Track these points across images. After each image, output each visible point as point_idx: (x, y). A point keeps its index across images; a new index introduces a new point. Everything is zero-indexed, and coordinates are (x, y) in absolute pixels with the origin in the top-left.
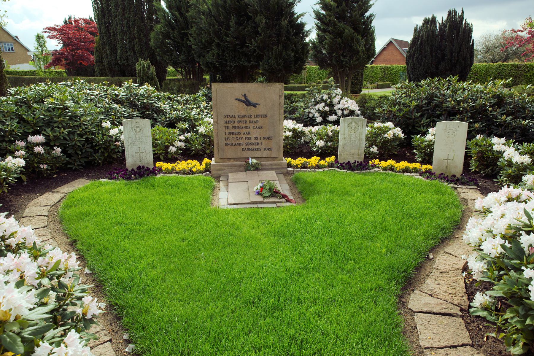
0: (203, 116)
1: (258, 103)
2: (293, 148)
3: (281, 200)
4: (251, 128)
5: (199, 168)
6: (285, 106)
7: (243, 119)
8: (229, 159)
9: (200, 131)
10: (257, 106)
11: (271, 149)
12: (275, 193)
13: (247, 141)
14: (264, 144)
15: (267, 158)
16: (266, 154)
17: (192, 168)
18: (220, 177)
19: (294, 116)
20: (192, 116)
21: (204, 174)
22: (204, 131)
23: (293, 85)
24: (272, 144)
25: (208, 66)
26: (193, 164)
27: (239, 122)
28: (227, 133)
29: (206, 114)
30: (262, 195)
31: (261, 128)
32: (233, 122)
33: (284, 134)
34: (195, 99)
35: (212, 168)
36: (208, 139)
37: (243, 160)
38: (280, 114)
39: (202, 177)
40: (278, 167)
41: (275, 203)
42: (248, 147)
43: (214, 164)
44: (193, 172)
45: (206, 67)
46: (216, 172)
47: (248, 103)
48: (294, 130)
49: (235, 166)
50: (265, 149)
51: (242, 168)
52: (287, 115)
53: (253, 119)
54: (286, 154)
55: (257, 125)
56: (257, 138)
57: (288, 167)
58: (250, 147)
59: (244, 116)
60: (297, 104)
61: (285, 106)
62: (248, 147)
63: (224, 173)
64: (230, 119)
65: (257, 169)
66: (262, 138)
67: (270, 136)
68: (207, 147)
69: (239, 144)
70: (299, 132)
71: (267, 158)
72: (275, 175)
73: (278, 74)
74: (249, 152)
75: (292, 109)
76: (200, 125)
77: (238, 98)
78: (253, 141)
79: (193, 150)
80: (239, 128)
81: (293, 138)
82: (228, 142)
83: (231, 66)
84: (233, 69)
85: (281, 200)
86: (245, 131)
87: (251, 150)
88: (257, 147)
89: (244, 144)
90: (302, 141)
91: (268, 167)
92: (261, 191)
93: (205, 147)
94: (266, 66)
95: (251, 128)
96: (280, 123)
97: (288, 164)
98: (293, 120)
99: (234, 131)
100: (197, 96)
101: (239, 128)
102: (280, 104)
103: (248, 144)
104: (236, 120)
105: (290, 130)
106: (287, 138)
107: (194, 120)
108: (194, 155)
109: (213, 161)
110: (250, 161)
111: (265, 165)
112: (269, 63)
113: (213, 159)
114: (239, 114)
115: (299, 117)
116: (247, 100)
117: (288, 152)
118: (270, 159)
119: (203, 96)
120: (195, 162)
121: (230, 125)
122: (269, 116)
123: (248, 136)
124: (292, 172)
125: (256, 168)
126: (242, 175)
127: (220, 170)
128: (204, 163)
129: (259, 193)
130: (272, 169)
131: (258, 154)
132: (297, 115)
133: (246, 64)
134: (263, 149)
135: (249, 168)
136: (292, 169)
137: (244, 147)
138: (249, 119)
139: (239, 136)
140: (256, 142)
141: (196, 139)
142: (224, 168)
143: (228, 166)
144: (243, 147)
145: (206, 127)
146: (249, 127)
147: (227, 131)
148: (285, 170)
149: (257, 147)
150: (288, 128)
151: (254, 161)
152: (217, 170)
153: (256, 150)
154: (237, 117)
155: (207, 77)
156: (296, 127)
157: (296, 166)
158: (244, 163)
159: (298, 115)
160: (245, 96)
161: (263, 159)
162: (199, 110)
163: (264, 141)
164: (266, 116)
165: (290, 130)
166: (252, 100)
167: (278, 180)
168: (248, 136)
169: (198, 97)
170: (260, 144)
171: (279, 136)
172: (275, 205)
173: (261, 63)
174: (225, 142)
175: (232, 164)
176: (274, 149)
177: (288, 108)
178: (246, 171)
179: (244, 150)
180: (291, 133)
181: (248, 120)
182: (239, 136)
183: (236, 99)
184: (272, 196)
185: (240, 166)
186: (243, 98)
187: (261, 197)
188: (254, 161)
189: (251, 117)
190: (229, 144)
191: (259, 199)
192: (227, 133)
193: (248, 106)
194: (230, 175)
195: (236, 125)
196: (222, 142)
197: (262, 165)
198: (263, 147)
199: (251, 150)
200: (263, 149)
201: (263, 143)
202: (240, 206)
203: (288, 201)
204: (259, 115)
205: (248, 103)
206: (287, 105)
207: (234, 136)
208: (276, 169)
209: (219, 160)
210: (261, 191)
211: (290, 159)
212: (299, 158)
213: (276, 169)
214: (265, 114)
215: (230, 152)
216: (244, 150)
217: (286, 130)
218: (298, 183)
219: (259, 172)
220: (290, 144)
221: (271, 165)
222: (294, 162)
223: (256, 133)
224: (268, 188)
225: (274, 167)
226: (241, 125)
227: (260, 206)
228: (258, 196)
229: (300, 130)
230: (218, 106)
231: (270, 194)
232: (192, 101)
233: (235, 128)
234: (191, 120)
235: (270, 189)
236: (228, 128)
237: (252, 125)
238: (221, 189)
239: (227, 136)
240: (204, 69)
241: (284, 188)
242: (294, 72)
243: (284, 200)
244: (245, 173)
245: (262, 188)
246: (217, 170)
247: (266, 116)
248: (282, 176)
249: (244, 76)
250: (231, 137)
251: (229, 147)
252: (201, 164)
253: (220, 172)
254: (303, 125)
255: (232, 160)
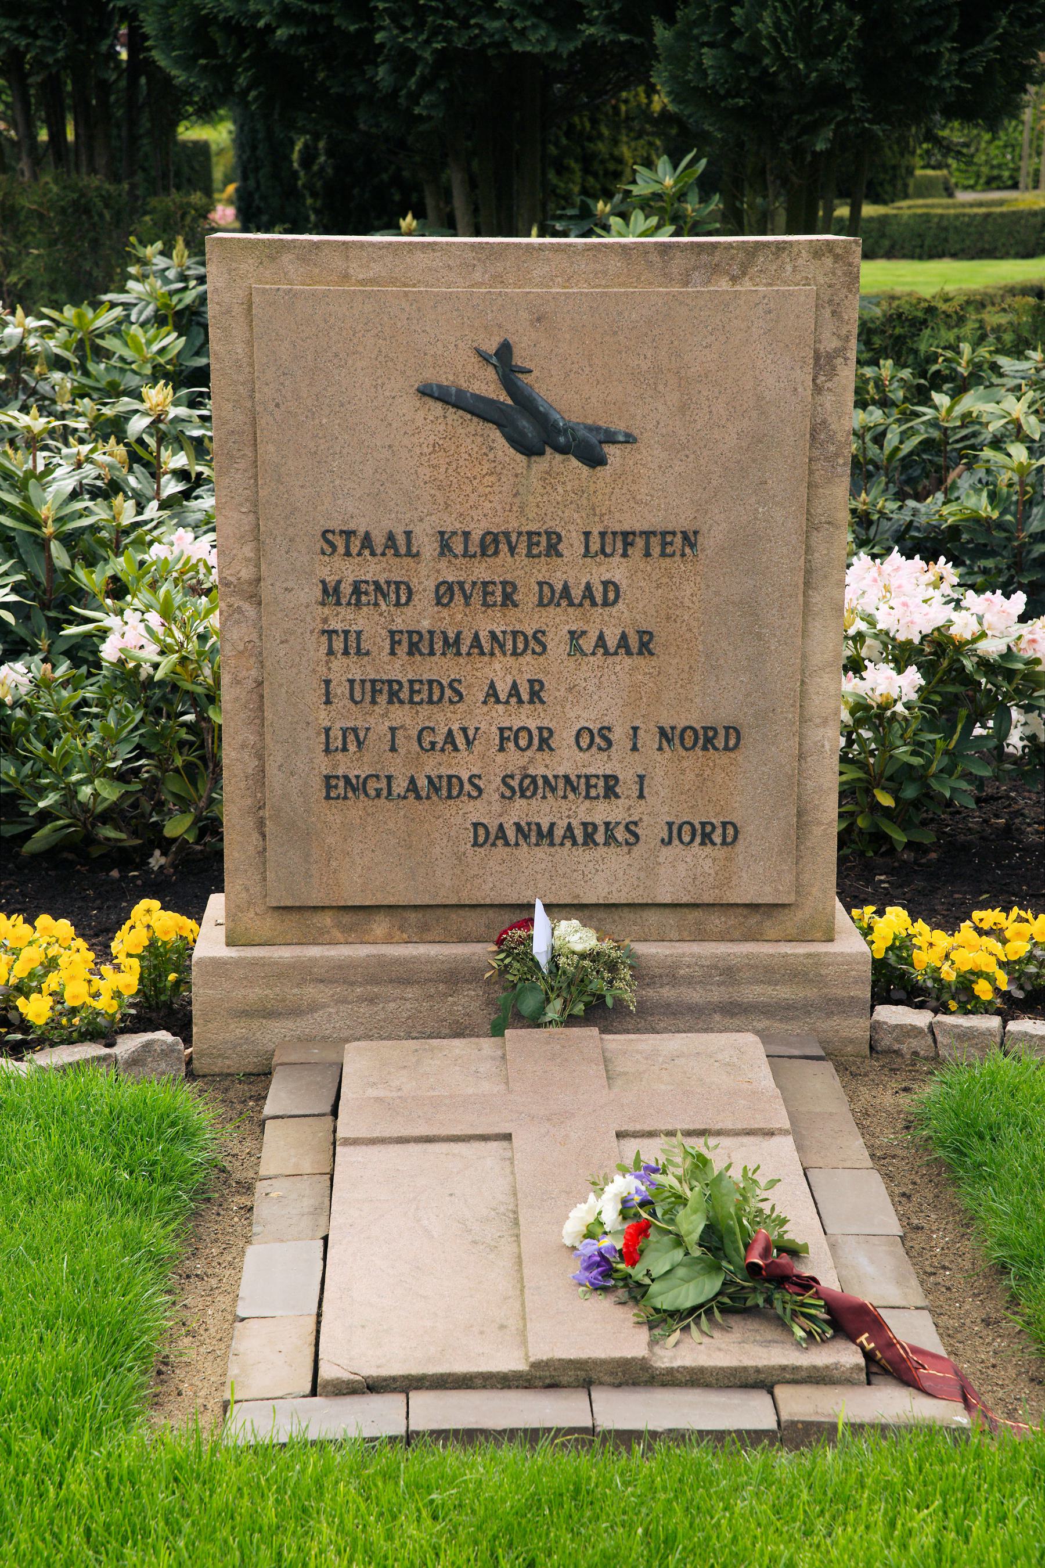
0: (152, 510)
1: (619, 425)
2: (922, 807)
3: (821, 1357)
4: (557, 645)
5: (76, 993)
6: (860, 418)
7: (481, 571)
8: (357, 915)
9: (109, 651)
10: (612, 451)
11: (730, 834)
12: (760, 1281)
13: (514, 760)
14: (670, 786)
15: (693, 912)
16: (681, 872)
17: (22, 989)
18: (267, 1074)
19: (935, 510)
20: (46, 511)
21: (128, 1045)
22: (151, 652)
23: (936, 206)
24: (741, 788)
25: (210, 51)
26: (31, 958)
27: (445, 594)
28: (340, 690)
29: (172, 487)
30: (637, 1292)
31: (646, 644)
32: (400, 593)
33: (850, 684)
34: (90, 348)
35: (201, 995)
36: (176, 720)
37: (474, 922)
38: (811, 526)
39: (101, 1082)
40: (784, 993)
41: (761, 1382)
42: (520, 811)
43: (217, 965)
44: (24, 1026)
45: (187, 63)
46: (238, 1030)
47: (529, 426)
48: (936, 655)
49: (404, 976)
50: (674, 834)
51: (468, 1001)
52: (878, 499)
53: (573, 570)
54: (869, 867)
55: (611, 624)
56: (605, 731)
57: (881, 996)
58: (543, 811)
59: (491, 544)
60: (972, 402)
61: (860, 418)
62: (520, 811)
63: (307, 1040)
64: (373, 570)
65: (598, 1012)
66: (649, 739)
67: (722, 717)
68: (174, 785)
69: (448, 788)
70: (985, 664)
71: (693, 912)
72: (763, 1076)
73: (812, 129)
74: (534, 859)
75: (927, 444)
76: (118, 589)
77: (445, 378)
78: (567, 760)
79: (45, 816)
80: (452, 645)
81: (930, 723)
82: (348, 766)
83: (404, 61)
84: (426, 84)
85: (821, 1357)
86: (502, 672)
87: (545, 836)
88: (602, 812)
89: (492, 786)
90: (1015, 741)
91: (695, 996)
92: (631, 1254)
93: (153, 786)
94: (708, 58)
95: (557, 645)
96: (815, 581)
97: (879, 965)
98: (930, 557)
99: (399, 669)
100: (105, 319)
101: (452, 645)
102: (817, 432)
103: (524, 787)
104: (426, 574)
105: (901, 655)
106: (869, 714)
107: (69, 540)
108: (51, 853)
109: (210, 937)
110: (544, 936)
111: (671, 974)
112: (735, 33)
113: (216, 903)
114: (451, 524)
115: (977, 522)
116: (525, 401)
117: (879, 838)
118: (716, 922)
119: (160, 320)
120: (56, 930)
121: (370, 623)
122: (709, 543)
123: (527, 718)
124: (923, 1045)
125: (592, 1000)
126: (464, 1071)
127: (268, 1013)
128: (127, 941)
129: (611, 1274)
130: (733, 1013)
131: (606, 875)
132: (968, 501)
133: (537, 40)
134: (652, 831)
135: (529, 1004)
136: (921, 1018)
137: (486, 810)
138: (542, 570)
139: (445, 719)
140: (598, 765)
141: (78, 710)
142: (311, 992)
143: (340, 975)
144: (477, 811)
145: (167, 614)
146: (538, 642)
147: (344, 670)
148: (854, 1029)
149: (602, 812)
150: (885, 637)
151: (579, 936)
152: (246, 1013)
153: (589, 839)
154: (429, 548)
155: (217, 135)
156: (963, 626)
157: (961, 994)
158: (482, 952)
159: (981, 505)
160: (503, 360)
161: (652, 917)
162: (110, 455)
163: (660, 764)
164: (690, 539)
165: (901, 655)
166: (567, 393)
167: (798, 1132)
168: (527, 718)
169: (116, 330)
170: (627, 787)
171: (803, 720)
172: (753, 1413)
173: (662, 34)
174: (323, 765)
175: (382, 962)
176: (749, 831)
177: (892, 439)
178: (497, 1031)
179: (486, 837)
180: (912, 678)
181: (525, 572)
182: (445, 719)
183: (426, 392)
184: (730, 1307)
185: (453, 977)
186: (487, 385)
187: (627, 1315)
188: (579, 936)
189: (553, 550)
190: (355, 787)
191: (610, 1332)
192: (340, 690)
193: (530, 450)
194: (359, 1062)
195: (422, 615)
196: (298, 769)
197: (642, 974)
198: (656, 813)
199: (545, 836)
200: (652, 831)
201: (659, 784)
202: (431, 1411)
203: (889, 1365)
204: (627, 538)
205: (529, 426)
206: (875, 415)
207: (400, 715)
208: (766, 1010)
209: (268, 925)
210: (631, 1254)
211: (895, 920)
212: (989, 917)
213: (766, 1010)
214: (681, 522)
215: (368, 856)
216: (486, 837)
217: (870, 647)
218: (979, 1174)
219: (614, 1041)
220: (900, 777)
221: (729, 973)
222: (944, 951)
223: (591, 694)
224: (691, 1224)
225: (753, 993)
226: (456, 619)
227: (618, 1410)
228: (604, 1304)
229: (992, 648)
230: (268, 451)
231: (711, 1286)
232: (59, 364)
233: (415, 644)
234: (43, 545)
235: (715, 1240)
236: (353, 645)
237: (559, 623)
238: (263, 1210)
239: (343, 715)
240: (180, 76)
241: (851, 1235)
242: (950, 113)
243: (847, 1356)
244: (488, 1045)
245: (640, 1223)
246: (246, 1013)
247: (690, 539)
248: (822, 1084)
249: (504, 153)
250: (380, 719)
251: (356, 808)
252: (104, 954)
253: (274, 1033)
254: (1020, 600)
255: (380, 926)
